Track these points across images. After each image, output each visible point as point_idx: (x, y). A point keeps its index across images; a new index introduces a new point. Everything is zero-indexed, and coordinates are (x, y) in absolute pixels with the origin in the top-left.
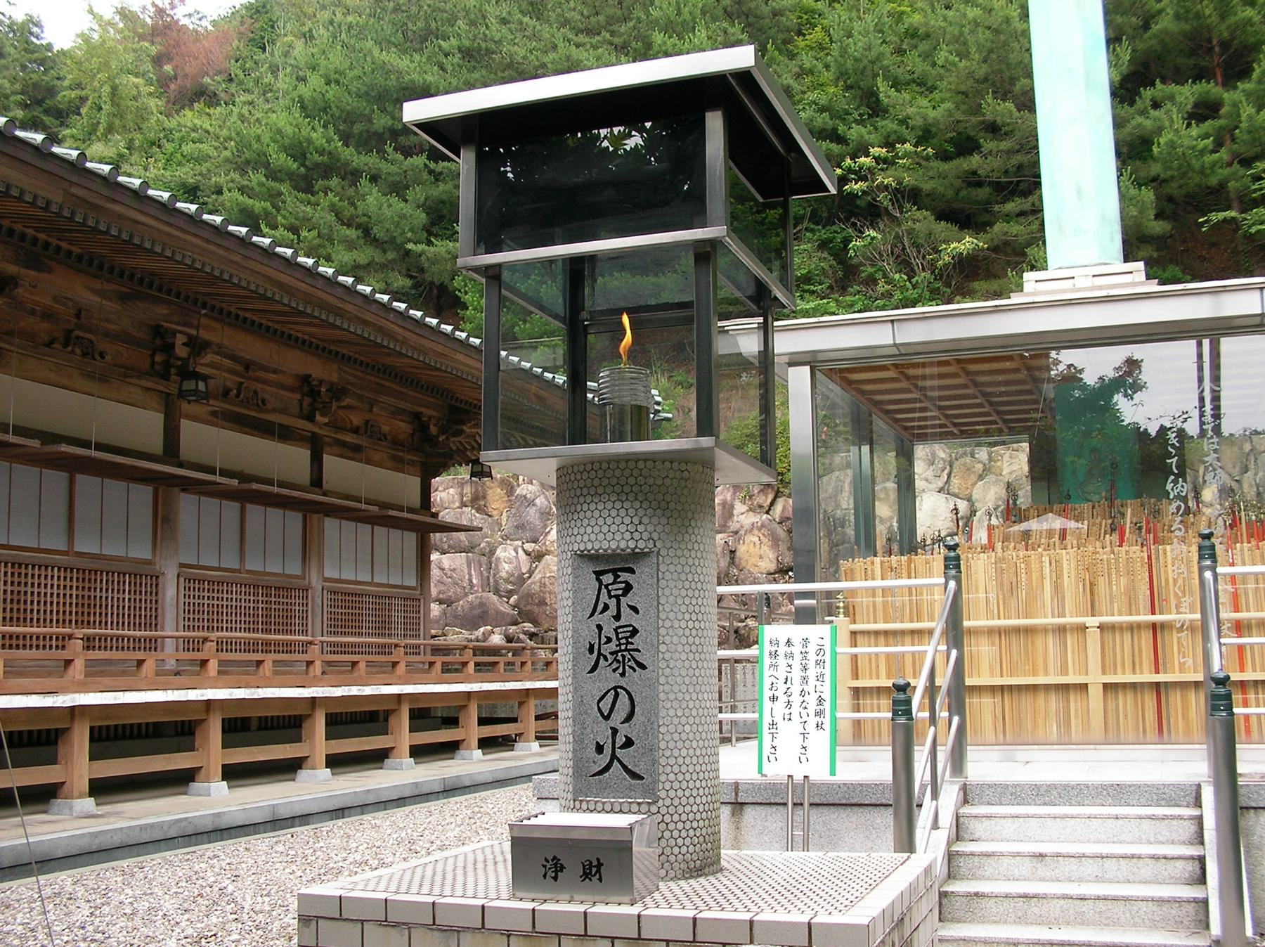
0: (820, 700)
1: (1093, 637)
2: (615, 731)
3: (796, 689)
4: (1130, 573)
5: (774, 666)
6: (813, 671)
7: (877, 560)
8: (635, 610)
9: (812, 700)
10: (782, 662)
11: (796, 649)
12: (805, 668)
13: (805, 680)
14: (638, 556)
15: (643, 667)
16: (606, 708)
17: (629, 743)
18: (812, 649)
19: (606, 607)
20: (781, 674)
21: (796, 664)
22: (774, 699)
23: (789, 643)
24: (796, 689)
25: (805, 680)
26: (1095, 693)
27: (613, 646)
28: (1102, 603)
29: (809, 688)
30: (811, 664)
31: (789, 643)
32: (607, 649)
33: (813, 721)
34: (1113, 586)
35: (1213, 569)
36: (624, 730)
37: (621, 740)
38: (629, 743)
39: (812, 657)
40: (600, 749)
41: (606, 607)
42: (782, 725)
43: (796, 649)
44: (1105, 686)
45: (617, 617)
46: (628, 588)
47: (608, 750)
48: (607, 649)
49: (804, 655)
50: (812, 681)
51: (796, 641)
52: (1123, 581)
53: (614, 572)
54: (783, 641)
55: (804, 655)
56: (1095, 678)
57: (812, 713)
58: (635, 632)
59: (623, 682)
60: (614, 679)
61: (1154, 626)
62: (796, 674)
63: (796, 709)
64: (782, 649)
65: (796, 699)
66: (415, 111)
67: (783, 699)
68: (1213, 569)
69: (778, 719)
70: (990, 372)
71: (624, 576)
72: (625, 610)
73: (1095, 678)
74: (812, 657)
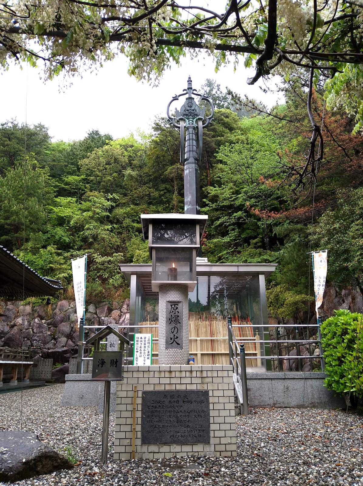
0: (149, 352)
1: (199, 342)
2: (174, 335)
3: (143, 349)
4: (206, 327)
5: (138, 344)
6: (147, 345)
7: (148, 322)
8: (178, 312)
9: (146, 352)
10: (139, 343)
11: (143, 340)
12: (145, 344)
13: (145, 347)
14: (179, 302)
15: (180, 323)
16: (172, 330)
17: (177, 338)
18: (147, 339)
19: (173, 312)
20: (139, 346)
21: (143, 343)
22: (137, 352)
23: (141, 338)
24: (143, 349)
25: (145, 347)
26: (199, 356)
27: (174, 319)
28: (200, 335)
29: (146, 349)
30: (146, 343)
31: (141, 338)
32: (173, 319)
33: (147, 357)
34: (202, 330)
35: (231, 325)
36: (176, 335)
37: (175, 337)
38: (177, 338)
39: (147, 342)
40: (171, 339)
41: (173, 312)
42: (139, 358)
43: (143, 340)
44: (201, 354)
45: (175, 314)
46: (177, 308)
47: (173, 339)
48: (173, 319)
49: (145, 341)
50: (147, 347)
51: (143, 338)
52: (204, 329)
53: (174, 305)
54: (140, 338)
55: (145, 341)
56: (199, 352)
57: (146, 355)
58: (178, 316)
59: (176, 326)
60: (174, 325)
61: (212, 340)
62: (143, 346)
63: (142, 354)
64: (140, 340)
65: (143, 352)
66: (143, 216)
67: (139, 352)
68: (231, 325)
69: (138, 357)
70: (147, 283)
71: (176, 306)
72: (177, 313)
73: (199, 352)
74: (147, 342)
